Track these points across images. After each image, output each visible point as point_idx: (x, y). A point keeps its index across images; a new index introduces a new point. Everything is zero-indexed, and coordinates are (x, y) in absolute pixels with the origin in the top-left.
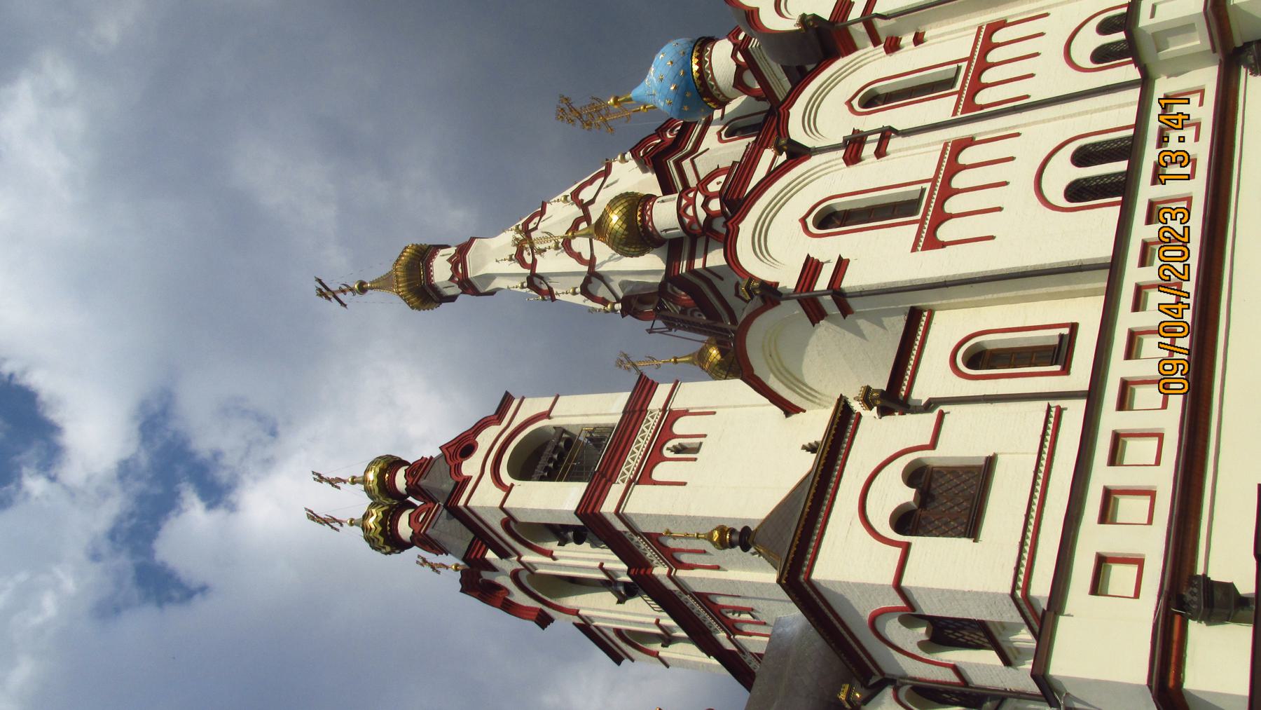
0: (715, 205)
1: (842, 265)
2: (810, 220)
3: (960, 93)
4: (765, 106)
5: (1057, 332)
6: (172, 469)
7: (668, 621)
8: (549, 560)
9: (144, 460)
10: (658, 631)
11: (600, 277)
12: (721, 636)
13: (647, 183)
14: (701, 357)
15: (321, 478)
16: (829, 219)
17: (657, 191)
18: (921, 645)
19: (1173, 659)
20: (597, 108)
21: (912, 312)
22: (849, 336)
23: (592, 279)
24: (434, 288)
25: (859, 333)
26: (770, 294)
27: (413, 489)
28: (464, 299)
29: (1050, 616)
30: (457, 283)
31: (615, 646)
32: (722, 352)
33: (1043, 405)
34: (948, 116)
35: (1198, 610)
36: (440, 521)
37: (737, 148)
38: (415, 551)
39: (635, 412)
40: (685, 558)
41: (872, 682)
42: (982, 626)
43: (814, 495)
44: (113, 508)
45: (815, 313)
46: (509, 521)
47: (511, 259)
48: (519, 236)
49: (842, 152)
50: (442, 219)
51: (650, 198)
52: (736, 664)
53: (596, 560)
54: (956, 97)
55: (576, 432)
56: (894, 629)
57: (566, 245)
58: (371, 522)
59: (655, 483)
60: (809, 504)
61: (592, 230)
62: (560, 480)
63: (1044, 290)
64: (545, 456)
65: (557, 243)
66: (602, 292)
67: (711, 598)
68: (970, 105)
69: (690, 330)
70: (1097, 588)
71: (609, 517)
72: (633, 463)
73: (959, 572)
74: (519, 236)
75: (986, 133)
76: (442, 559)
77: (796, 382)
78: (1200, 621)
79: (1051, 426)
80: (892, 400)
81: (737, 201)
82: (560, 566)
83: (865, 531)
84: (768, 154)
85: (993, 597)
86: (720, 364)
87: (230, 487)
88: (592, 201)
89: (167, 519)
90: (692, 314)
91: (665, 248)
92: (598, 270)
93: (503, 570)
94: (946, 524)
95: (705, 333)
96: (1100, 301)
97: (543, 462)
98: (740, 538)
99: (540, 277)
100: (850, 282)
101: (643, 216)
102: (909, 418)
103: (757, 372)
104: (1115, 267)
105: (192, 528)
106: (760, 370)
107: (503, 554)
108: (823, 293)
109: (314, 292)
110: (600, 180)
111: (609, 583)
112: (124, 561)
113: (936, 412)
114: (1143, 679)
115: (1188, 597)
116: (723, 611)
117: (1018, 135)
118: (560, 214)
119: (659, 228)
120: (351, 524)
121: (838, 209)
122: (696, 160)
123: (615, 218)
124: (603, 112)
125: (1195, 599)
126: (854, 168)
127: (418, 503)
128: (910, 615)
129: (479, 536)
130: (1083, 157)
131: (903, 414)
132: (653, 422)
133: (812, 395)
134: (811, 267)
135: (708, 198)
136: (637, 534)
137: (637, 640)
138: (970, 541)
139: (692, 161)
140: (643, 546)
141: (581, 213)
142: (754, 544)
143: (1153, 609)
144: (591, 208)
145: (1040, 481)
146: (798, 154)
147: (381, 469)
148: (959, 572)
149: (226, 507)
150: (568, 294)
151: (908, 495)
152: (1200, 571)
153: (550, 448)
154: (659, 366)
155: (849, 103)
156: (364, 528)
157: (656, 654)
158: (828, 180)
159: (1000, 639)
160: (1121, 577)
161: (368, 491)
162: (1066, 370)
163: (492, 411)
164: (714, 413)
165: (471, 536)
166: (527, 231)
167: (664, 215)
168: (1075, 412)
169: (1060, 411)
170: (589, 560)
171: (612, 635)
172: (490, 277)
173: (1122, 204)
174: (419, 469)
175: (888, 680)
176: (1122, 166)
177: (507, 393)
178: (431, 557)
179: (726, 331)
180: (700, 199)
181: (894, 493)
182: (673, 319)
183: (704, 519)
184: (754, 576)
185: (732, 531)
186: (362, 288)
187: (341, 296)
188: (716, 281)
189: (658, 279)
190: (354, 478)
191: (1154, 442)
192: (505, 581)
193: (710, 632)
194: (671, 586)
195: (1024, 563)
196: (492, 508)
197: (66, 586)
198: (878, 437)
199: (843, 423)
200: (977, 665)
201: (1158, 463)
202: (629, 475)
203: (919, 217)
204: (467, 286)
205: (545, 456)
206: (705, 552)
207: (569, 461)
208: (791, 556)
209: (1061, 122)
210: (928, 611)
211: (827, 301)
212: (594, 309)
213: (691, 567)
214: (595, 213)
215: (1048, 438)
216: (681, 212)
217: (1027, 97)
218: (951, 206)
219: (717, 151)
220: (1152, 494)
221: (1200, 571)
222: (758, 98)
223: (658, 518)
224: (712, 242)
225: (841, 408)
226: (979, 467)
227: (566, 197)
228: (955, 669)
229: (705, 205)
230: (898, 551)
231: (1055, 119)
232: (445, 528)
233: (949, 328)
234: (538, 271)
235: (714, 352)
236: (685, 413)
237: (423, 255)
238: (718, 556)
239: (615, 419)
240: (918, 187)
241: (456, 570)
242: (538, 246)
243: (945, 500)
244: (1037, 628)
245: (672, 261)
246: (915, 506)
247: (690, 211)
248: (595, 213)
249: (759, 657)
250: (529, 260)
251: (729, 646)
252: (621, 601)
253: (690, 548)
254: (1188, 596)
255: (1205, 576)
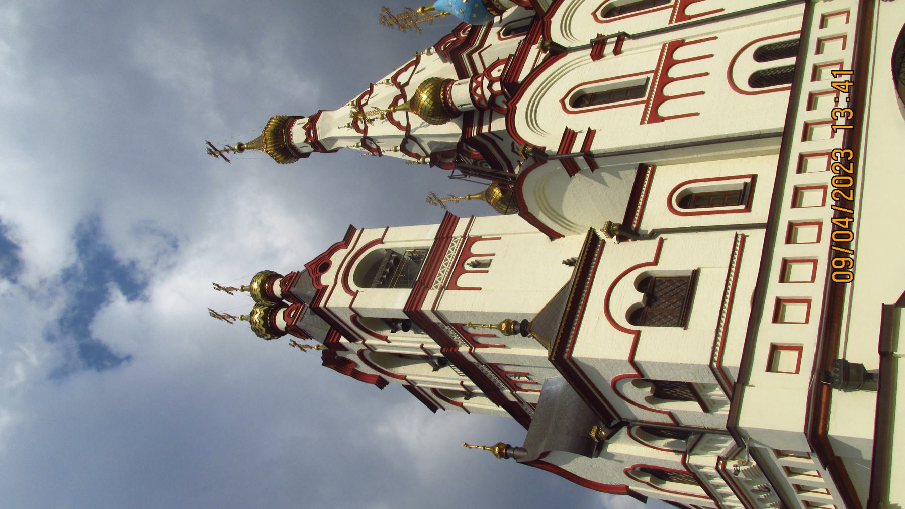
0: (497, 87)
1: (591, 134)
2: (567, 101)
3: (674, 6)
4: (532, 13)
5: (742, 181)
6: (101, 272)
7: (469, 383)
8: (385, 343)
9: (81, 266)
10: (462, 389)
11: (415, 139)
12: (507, 392)
13: (447, 70)
14: (488, 195)
15: (219, 288)
16: (581, 100)
17: (455, 77)
18: (648, 399)
19: (822, 416)
20: (409, 13)
21: (642, 167)
22: (596, 184)
23: (408, 140)
24: (294, 148)
25: (602, 181)
26: (539, 155)
27: (286, 295)
28: (315, 155)
29: (739, 386)
30: (310, 144)
31: (433, 400)
32: (503, 192)
33: (732, 233)
34: (666, 24)
35: (839, 383)
36: (306, 316)
37: (512, 44)
38: (288, 337)
39: (444, 238)
40: (481, 340)
41: (613, 424)
42: (689, 386)
43: (573, 298)
44: (61, 302)
45: (572, 168)
46: (356, 317)
47: (349, 126)
48: (355, 110)
49: (589, 51)
50: (293, 91)
51: (450, 82)
52: (517, 411)
53: (418, 342)
54: (671, 9)
55: (402, 253)
56: (628, 389)
57: (389, 116)
58: (256, 317)
59: (459, 289)
60: (570, 305)
61: (408, 106)
62: (391, 287)
63: (733, 151)
64: (381, 269)
65: (382, 115)
66: (416, 149)
67: (499, 367)
68: (681, 16)
69: (479, 176)
70: (771, 366)
71: (427, 313)
72: (443, 275)
73: (672, 349)
74: (355, 110)
75: (693, 37)
76: (308, 342)
77: (558, 216)
78: (840, 390)
79: (737, 248)
80: (627, 230)
81: (513, 89)
82: (393, 347)
83: (612, 327)
84: (534, 50)
85: (698, 367)
86: (501, 199)
87: (145, 284)
88: (407, 84)
89: (99, 308)
90: (481, 165)
91: (461, 118)
92: (412, 133)
93: (352, 350)
94: (665, 317)
95: (490, 179)
96: (776, 157)
97: (379, 274)
98: (522, 328)
99: (371, 139)
100: (595, 147)
101: (445, 95)
102: (639, 243)
103: (530, 210)
104: (786, 135)
105: (117, 316)
106: (532, 208)
107: (352, 339)
108: (577, 155)
109: (205, 152)
110: (413, 68)
111: (428, 357)
112: (71, 341)
113: (658, 238)
114: (802, 431)
115: (833, 374)
116: (508, 375)
117: (715, 38)
118: (383, 94)
119: (456, 104)
120: (242, 319)
121: (587, 93)
122: (482, 54)
123: (424, 97)
124: (414, 18)
125: (837, 375)
126: (599, 63)
127: (289, 304)
128: (640, 379)
129: (334, 326)
130: (762, 55)
131: (634, 240)
132: (456, 246)
133: (570, 226)
134: (569, 136)
135: (492, 82)
136: (447, 324)
137: (447, 395)
138: (682, 329)
139: (480, 54)
140: (451, 332)
141: (399, 93)
142: (531, 331)
143: (809, 381)
144: (406, 89)
145: (730, 287)
146: (556, 52)
147: (262, 281)
148: (672, 349)
149: (141, 300)
150: (391, 151)
151: (638, 297)
152: (840, 357)
153: (383, 265)
154: (457, 201)
155: (594, 14)
156: (251, 322)
157: (461, 405)
158: (579, 71)
159: (701, 394)
160: (787, 359)
161: (253, 296)
162: (748, 209)
163: (340, 238)
164: (500, 238)
165: (329, 327)
166: (360, 106)
167: (460, 94)
168: (756, 239)
169: (744, 237)
170: (413, 342)
171: (430, 392)
172: (334, 139)
173: (792, 89)
174: (290, 280)
175: (625, 423)
176: (791, 61)
177: (351, 226)
178: (300, 341)
179: (506, 177)
180: (486, 82)
181: (629, 296)
182: (467, 169)
183: (494, 313)
184: (531, 353)
185: (515, 323)
186: (241, 148)
187: (225, 154)
188: (498, 141)
189: (456, 140)
190: (243, 287)
191: (811, 266)
192: (353, 357)
193: (499, 390)
194: (471, 359)
195: (719, 343)
196: (344, 308)
197: (31, 358)
198: (617, 257)
199: (593, 247)
200: (685, 412)
201: (813, 280)
202: (440, 283)
203: (645, 99)
204: (318, 146)
205: (381, 269)
206: (495, 336)
207: (398, 273)
208: (558, 341)
209: (745, 29)
210: (652, 377)
211: (581, 161)
212: (410, 162)
213: (486, 346)
214: (410, 93)
215: (736, 256)
216: (472, 92)
217: (722, 10)
218: (668, 90)
219: (498, 46)
220: (808, 302)
221: (840, 357)
222: (527, 8)
223: (462, 313)
224: (494, 113)
225: (591, 237)
226: (688, 278)
227: (388, 80)
228: (670, 414)
229: (490, 87)
230: (632, 337)
231: (742, 27)
232: (309, 320)
233: (667, 178)
234: (368, 135)
235: (497, 191)
236: (479, 238)
237: (283, 125)
238: (504, 339)
239: (429, 243)
240: (644, 77)
241: (318, 349)
242: (369, 117)
243: (665, 300)
244: (731, 394)
245: (466, 127)
246: (644, 305)
247: (479, 91)
248: (410, 93)
249: (533, 406)
250: (362, 126)
251: (512, 399)
252: (436, 369)
253: (485, 333)
254: (832, 374)
255: (844, 359)
